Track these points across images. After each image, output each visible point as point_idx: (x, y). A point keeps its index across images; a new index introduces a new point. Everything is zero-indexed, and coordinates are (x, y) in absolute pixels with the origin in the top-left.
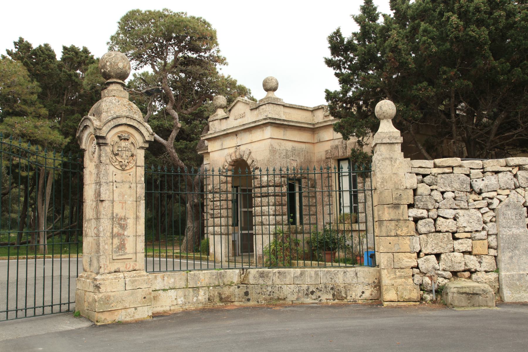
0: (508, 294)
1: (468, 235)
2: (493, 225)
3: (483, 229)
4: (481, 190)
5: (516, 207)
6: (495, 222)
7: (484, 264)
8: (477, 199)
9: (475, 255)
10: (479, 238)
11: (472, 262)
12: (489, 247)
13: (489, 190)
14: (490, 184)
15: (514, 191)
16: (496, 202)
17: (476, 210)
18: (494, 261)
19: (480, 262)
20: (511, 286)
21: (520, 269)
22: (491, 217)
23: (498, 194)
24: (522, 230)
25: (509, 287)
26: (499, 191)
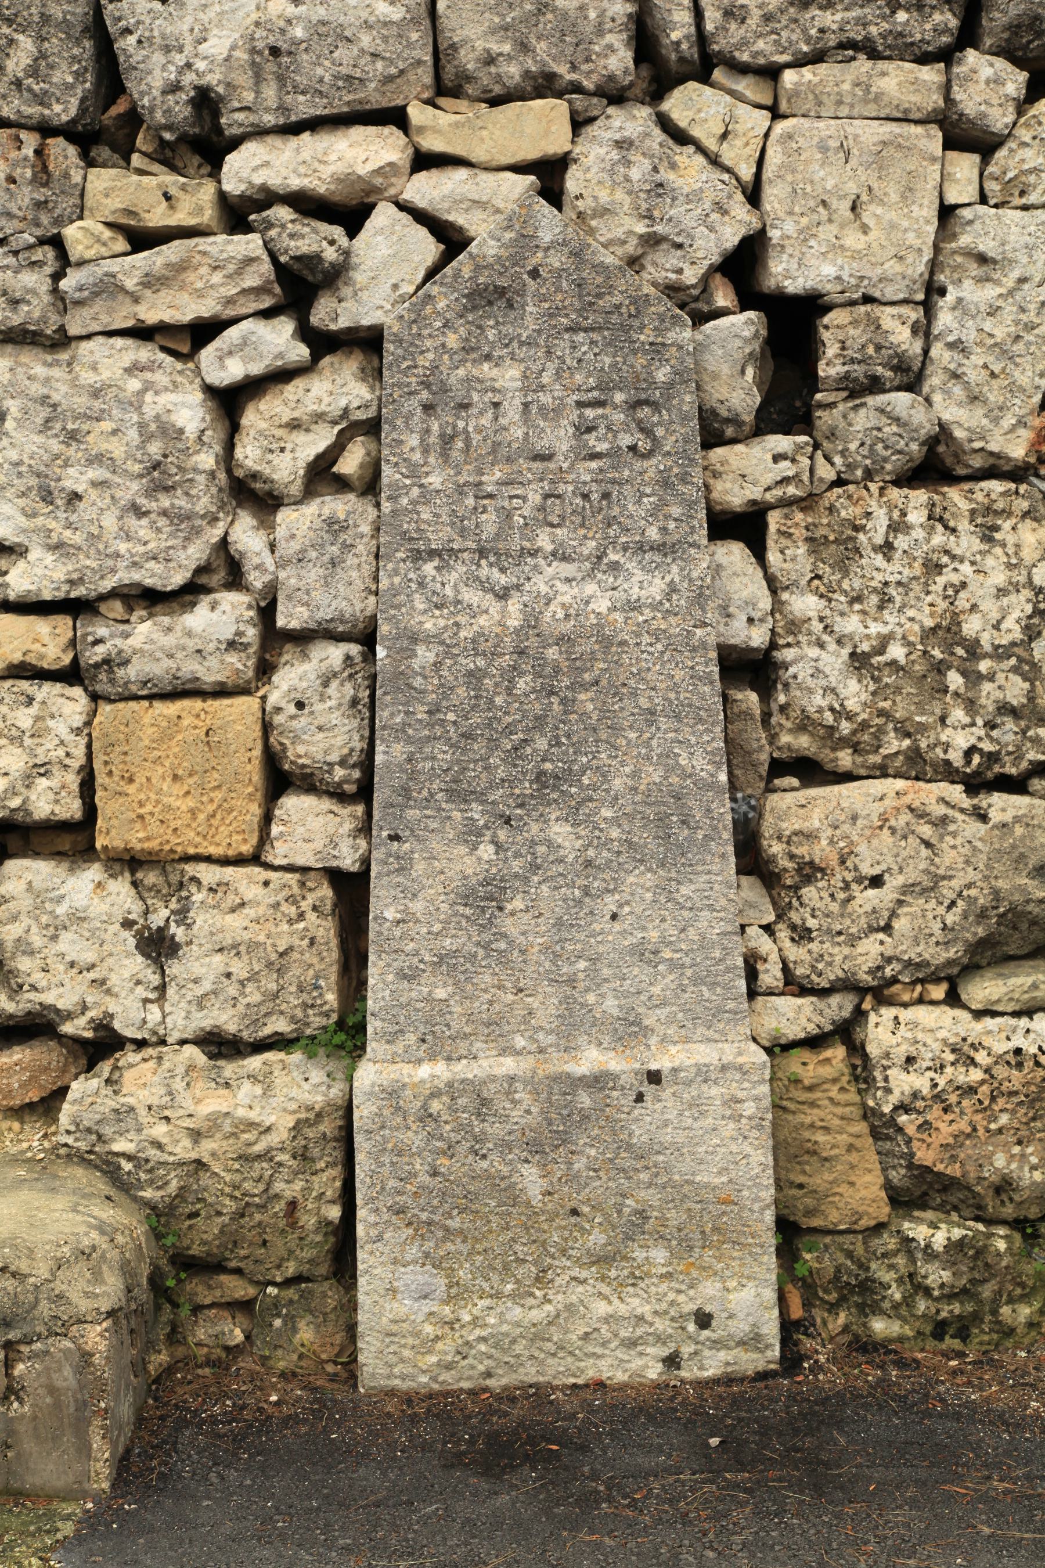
0: (403, 1306)
1: (46, 640)
2: (334, 526)
3: (227, 568)
4: (206, 102)
5: (595, 308)
6: (370, 485)
7: (197, 965)
8: (157, 217)
9: (130, 862)
10: (159, 669)
11: (71, 945)
12: (280, 779)
13: (304, 107)
14: (320, 30)
15: (633, 121)
16: (387, 258)
17: (145, 352)
18: (326, 930)
19: (158, 946)
20: (465, 1219)
21: (573, 1024)
22: (321, 440)
23: (424, 161)
24: (646, 584)
25: (422, 1229)
26: (417, 113)
